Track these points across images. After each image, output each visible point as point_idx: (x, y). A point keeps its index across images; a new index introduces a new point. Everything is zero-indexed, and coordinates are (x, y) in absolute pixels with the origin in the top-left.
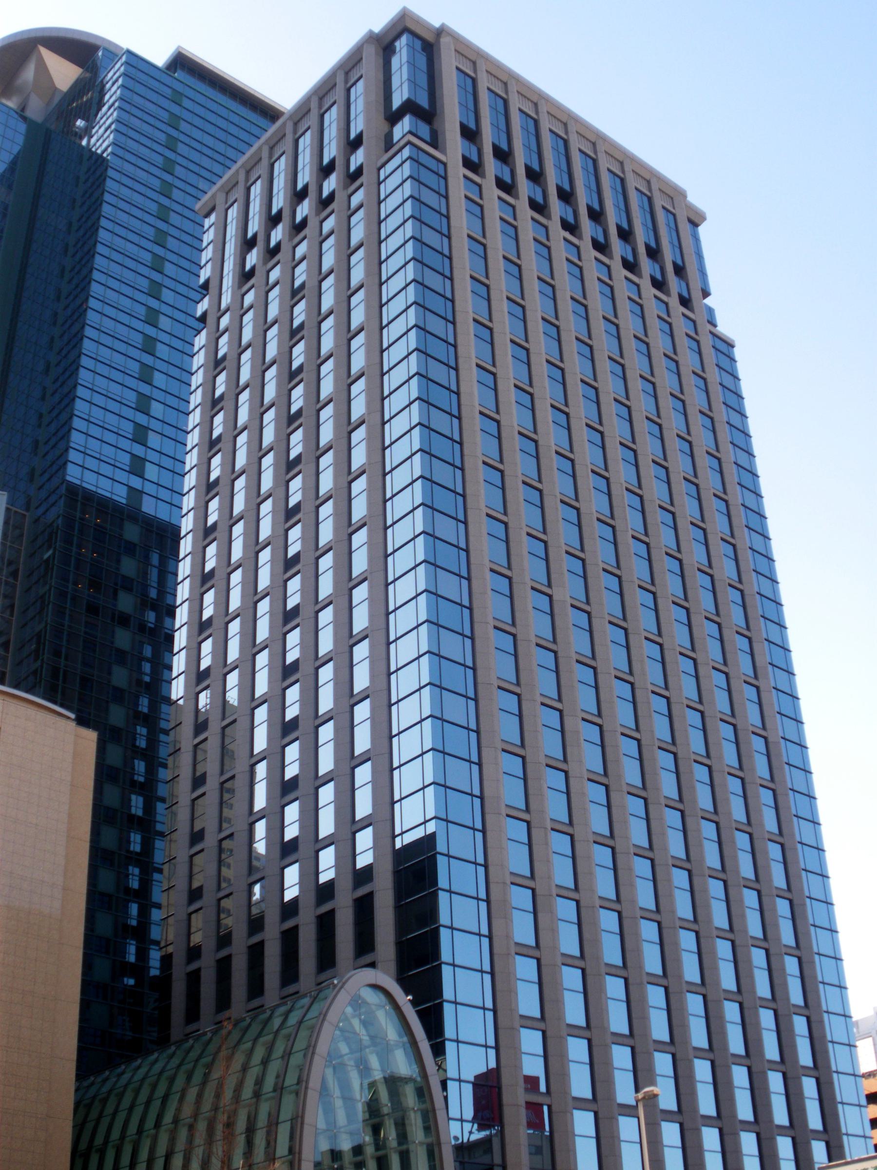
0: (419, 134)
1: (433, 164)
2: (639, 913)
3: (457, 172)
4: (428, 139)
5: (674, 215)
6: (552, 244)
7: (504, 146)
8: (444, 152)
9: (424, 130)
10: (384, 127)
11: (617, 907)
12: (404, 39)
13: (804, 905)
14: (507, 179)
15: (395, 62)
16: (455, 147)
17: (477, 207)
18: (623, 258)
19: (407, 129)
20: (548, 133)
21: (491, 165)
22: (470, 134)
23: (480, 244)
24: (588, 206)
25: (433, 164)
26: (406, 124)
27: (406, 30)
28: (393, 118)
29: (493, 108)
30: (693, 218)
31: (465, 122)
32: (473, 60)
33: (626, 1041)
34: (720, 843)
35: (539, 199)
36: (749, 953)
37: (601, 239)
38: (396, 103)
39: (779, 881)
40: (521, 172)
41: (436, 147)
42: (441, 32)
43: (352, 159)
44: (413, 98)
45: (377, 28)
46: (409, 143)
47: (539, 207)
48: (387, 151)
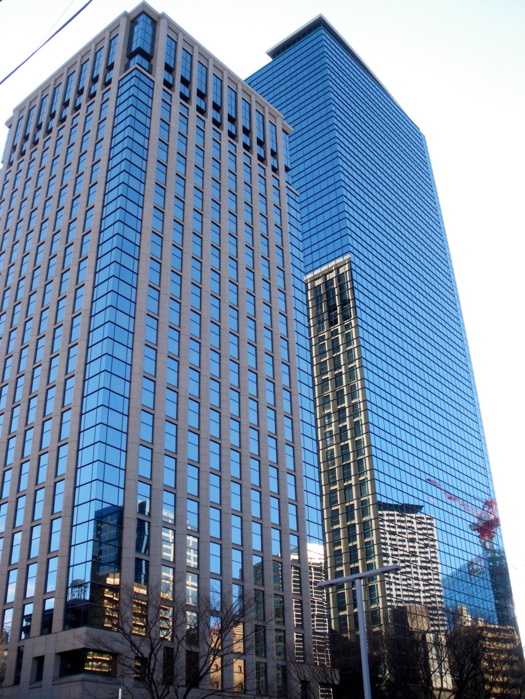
0: (143, 65)
1: (147, 81)
2: (271, 526)
3: (159, 85)
4: (147, 69)
5: (275, 126)
6: (206, 130)
7: (233, 116)
8: (279, 175)
9: (145, 64)
10: (127, 60)
11: (279, 528)
12: (143, 17)
13: (304, 509)
14: (234, 132)
15: (136, 28)
16: (160, 74)
17: (167, 104)
18: (244, 143)
19: (136, 62)
20: (197, 63)
21: (179, 86)
22: (169, 69)
23: (166, 123)
24: (214, 102)
25: (147, 81)
26: (138, 58)
27: (143, 12)
28: (130, 56)
29: (200, 72)
30: (285, 130)
31: (168, 63)
32: (174, 30)
33: (218, 577)
34: (295, 486)
35: (248, 144)
36: (288, 538)
37: (262, 155)
38: (134, 48)
39: (291, 495)
40: (240, 129)
41: (151, 74)
42: (163, 16)
43: (108, 75)
44: (142, 47)
45: (129, 10)
46: (136, 68)
47: (217, 124)
48: (125, 71)
